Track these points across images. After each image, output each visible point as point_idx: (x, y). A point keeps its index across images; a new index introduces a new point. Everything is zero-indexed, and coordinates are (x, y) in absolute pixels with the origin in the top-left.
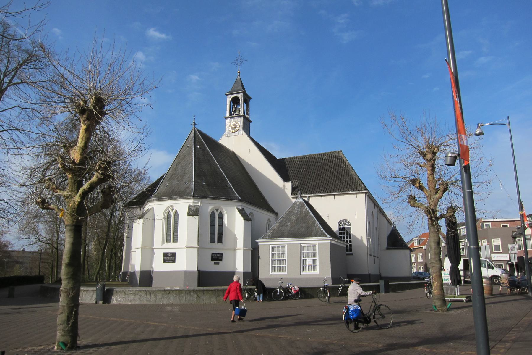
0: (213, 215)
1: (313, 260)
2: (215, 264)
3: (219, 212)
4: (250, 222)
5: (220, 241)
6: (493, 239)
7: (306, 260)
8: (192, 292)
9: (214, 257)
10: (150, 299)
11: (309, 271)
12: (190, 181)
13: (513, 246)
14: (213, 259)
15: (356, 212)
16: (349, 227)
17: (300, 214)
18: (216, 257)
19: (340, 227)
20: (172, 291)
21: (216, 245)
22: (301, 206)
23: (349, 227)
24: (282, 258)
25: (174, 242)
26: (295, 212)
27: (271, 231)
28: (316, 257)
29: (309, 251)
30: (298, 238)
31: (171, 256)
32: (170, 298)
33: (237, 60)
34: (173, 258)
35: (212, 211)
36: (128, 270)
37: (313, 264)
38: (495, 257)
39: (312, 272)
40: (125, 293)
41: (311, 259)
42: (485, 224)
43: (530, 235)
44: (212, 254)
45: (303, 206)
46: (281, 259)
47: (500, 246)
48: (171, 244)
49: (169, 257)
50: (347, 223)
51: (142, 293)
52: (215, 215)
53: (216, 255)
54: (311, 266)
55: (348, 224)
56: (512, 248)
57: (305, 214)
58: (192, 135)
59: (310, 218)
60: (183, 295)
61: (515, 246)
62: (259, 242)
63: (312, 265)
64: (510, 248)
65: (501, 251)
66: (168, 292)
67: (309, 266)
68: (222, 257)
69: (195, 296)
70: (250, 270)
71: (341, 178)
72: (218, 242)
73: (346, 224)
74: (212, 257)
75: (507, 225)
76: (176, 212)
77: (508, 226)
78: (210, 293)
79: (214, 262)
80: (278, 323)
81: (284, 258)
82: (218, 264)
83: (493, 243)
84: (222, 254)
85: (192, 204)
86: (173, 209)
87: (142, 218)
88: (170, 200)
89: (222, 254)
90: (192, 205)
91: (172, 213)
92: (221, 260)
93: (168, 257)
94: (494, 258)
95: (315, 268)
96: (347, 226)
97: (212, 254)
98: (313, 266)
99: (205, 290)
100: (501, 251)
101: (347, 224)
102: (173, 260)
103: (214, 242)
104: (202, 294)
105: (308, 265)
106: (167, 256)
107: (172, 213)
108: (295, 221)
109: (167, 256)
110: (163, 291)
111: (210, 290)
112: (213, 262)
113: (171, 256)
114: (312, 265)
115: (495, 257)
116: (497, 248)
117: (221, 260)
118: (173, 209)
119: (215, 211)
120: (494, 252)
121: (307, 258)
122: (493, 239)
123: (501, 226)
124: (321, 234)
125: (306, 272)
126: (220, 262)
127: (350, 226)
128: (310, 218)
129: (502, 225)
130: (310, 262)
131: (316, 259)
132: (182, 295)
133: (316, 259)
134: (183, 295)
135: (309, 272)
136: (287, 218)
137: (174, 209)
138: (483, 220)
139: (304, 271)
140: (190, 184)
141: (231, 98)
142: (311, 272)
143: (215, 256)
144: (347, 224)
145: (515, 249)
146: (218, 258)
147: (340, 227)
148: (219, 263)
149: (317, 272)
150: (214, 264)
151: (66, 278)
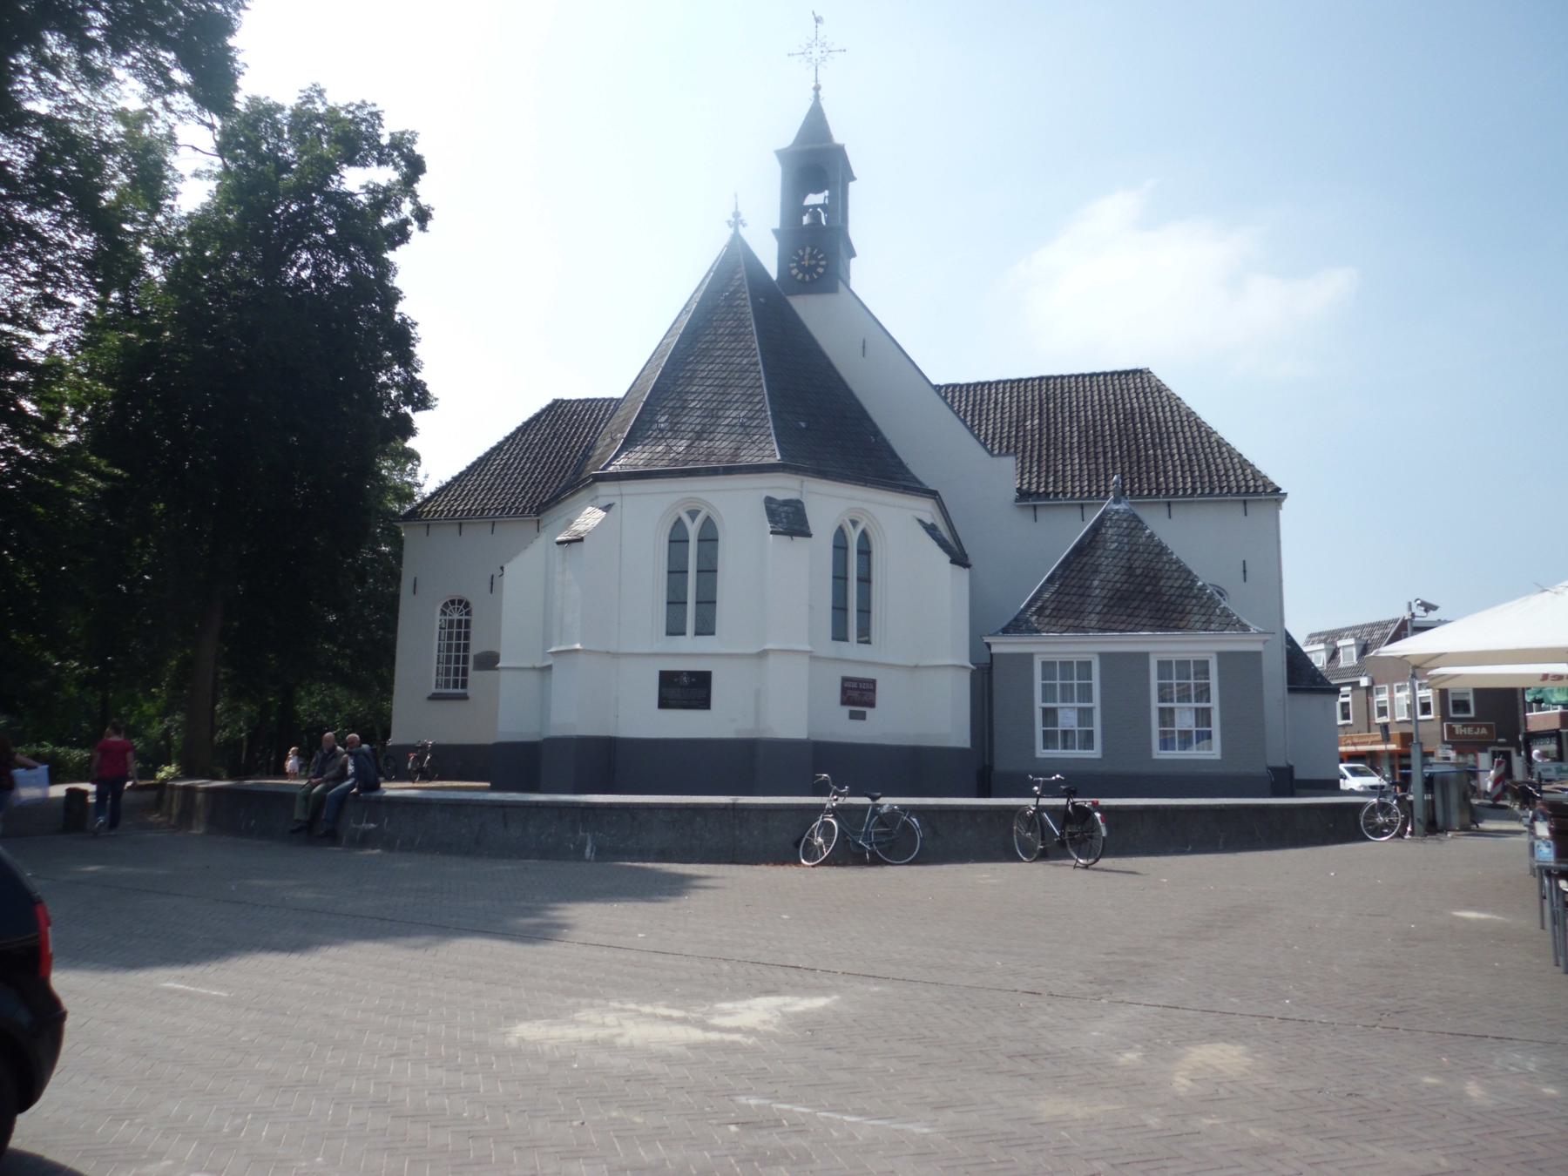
0: (677, 539)
1: (1080, 710)
2: (853, 715)
3: (700, 519)
4: (967, 569)
5: (865, 635)
7: (1172, 710)
9: (850, 693)
14: (846, 700)
16: (467, 617)
21: (852, 649)
23: (467, 617)
35: (834, 530)
41: (1074, 708)
44: (845, 680)
47: (1386, 707)
50: (461, 607)
52: (688, 536)
53: (855, 685)
54: (1074, 731)
62: (995, 643)
65: (1472, 714)
67: (1065, 733)
68: (874, 691)
74: (844, 690)
80: (1442, 766)
82: (862, 716)
84: (873, 682)
86: (854, 523)
89: (873, 682)
91: (693, 530)
92: (872, 704)
95: (1087, 741)
96: (462, 615)
97: (845, 680)
101: (462, 611)
103: (845, 639)
107: (693, 530)
112: (847, 709)
117: (872, 704)
118: (693, 514)
119: (686, 519)
120: (1452, 715)
121: (1058, 704)
126: (868, 710)
137: (698, 512)
143: (851, 689)
144: (458, 609)
148: (864, 713)
149: (1096, 752)
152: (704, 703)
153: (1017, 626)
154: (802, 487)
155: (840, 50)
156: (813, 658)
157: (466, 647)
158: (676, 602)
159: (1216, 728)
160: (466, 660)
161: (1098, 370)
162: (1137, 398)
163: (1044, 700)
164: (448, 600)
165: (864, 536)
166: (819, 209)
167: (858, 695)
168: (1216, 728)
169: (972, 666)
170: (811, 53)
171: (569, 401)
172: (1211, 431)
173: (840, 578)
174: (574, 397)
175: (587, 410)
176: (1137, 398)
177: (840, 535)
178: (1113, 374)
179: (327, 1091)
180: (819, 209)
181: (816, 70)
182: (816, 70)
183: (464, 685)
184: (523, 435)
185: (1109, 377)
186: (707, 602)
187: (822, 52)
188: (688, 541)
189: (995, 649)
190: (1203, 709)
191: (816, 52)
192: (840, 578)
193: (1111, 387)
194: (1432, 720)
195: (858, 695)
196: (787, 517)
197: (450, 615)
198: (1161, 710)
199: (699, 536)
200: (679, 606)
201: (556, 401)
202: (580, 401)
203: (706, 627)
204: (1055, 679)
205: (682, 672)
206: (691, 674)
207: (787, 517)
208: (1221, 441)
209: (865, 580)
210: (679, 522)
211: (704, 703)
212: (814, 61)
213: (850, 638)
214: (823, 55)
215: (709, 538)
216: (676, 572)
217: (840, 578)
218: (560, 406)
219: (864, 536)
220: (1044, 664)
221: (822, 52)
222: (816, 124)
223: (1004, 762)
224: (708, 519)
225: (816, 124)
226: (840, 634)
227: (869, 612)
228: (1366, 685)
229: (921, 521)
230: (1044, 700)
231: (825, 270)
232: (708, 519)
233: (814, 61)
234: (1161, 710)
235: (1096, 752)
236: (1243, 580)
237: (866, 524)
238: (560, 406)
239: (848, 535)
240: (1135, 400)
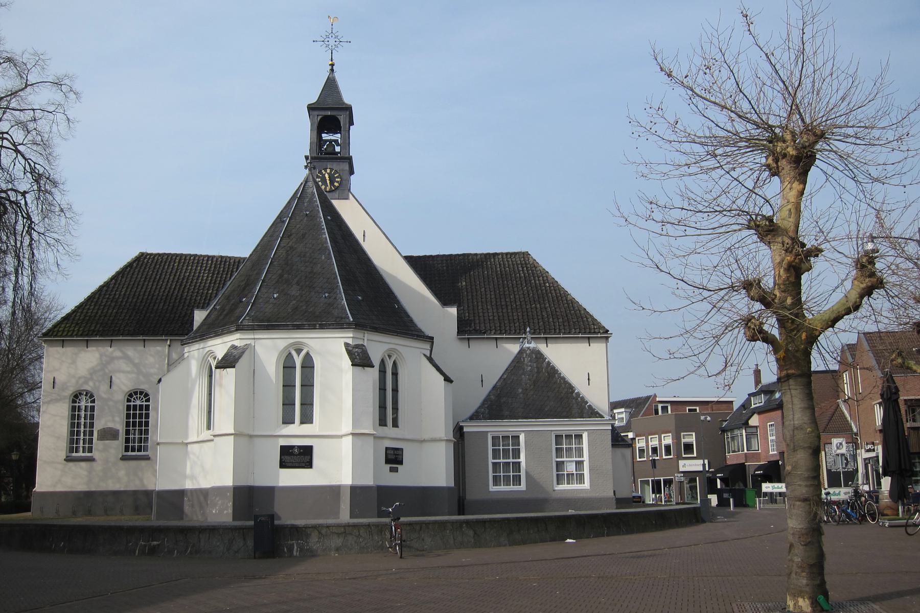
0: (288, 367)
2: (392, 470)
3: (303, 353)
5: (395, 424)
6: (682, 434)
7: (563, 462)
8: (464, 525)
10: (381, 543)
11: (568, 483)
12: (333, 289)
13: (840, 442)
14: (388, 461)
15: (54, 378)
17: (538, 372)
18: (393, 457)
19: (129, 403)
20: (426, 524)
21: (389, 431)
22: (536, 358)
24: (576, 457)
25: (302, 423)
26: (527, 368)
27: (486, 406)
28: (583, 457)
29: (571, 447)
30: (547, 420)
31: (300, 454)
32: (423, 540)
33: (336, 37)
34: (307, 458)
36: (278, 482)
37: (576, 471)
38: (685, 464)
39: (512, 488)
40: (320, 533)
41: (572, 461)
42: (660, 406)
43: (756, 427)
45: (540, 358)
46: (511, 460)
48: (297, 429)
49: (297, 455)
50: (142, 396)
51: (362, 531)
55: (144, 399)
56: (838, 445)
57: (548, 373)
58: (309, 191)
59: (560, 381)
60: (448, 531)
61: (843, 441)
63: (575, 472)
64: (844, 447)
65: (695, 455)
66: (418, 528)
67: (568, 475)
69: (471, 533)
70: (452, 484)
71: (205, 300)
72: (393, 426)
73: (137, 397)
75: (696, 409)
76: (308, 355)
77: (698, 411)
78: (495, 526)
79: (390, 467)
81: (562, 458)
82: (395, 470)
83: (683, 441)
85: (350, 341)
86: (390, 356)
87: (234, 367)
88: (297, 329)
90: (351, 343)
91: (298, 361)
92: (401, 463)
93: (294, 455)
94: (683, 466)
95: (581, 479)
96: (143, 402)
98: (576, 474)
99: (488, 521)
100: (695, 455)
101: (142, 399)
102: (308, 462)
103: (386, 425)
104: (483, 530)
105: (565, 473)
106: (292, 454)
107: (298, 361)
108: (530, 386)
109: (292, 454)
110: (407, 524)
111: (495, 521)
112: (388, 466)
113: (300, 454)
114: (575, 472)
115: (685, 464)
116: (688, 448)
117: (401, 463)
118: (299, 351)
120: (684, 456)
122: (682, 434)
123: (686, 411)
124: (591, 413)
125: (564, 487)
126: (399, 467)
127: (149, 402)
128: (560, 381)
129: (687, 408)
130: (571, 468)
131: (582, 462)
132: (446, 533)
133: (582, 462)
134: (448, 531)
135: (568, 486)
136: (513, 379)
138: (658, 399)
139: (558, 484)
140: (335, 298)
141: (319, 118)
142: (573, 485)
144: (140, 397)
145: (842, 447)
146: (396, 458)
147: (129, 403)
149: (586, 485)
150: (390, 471)
151: (812, 475)
152: (309, 465)
153: (475, 417)
154: (364, 337)
155: (347, 42)
156: (353, 434)
157: (92, 425)
158: (288, 403)
159: (586, 472)
160: (91, 433)
161: (498, 251)
162: (523, 270)
163: (494, 458)
164: (127, 397)
165: (395, 364)
166: (333, 143)
167: (394, 458)
168: (586, 472)
169: (454, 439)
170: (328, 41)
171: (151, 254)
172: (567, 294)
173: (382, 389)
174: (155, 251)
175: (166, 262)
176: (523, 270)
177: (383, 362)
178: (507, 254)
179: (802, 436)
180: (333, 143)
181: (332, 53)
182: (332, 53)
183: (90, 450)
184: (122, 277)
185: (505, 256)
186: (308, 404)
187: (336, 41)
188: (295, 367)
189: (465, 430)
190: (516, 462)
191: (332, 42)
192: (382, 389)
193: (507, 263)
194: (645, 461)
195: (394, 458)
196: (358, 355)
197: (79, 403)
198: (494, 464)
199: (302, 364)
200: (290, 406)
201: (142, 254)
202: (159, 255)
203: (307, 418)
204: (131, 411)
205: (295, 446)
206: (300, 447)
207: (358, 355)
208: (573, 300)
209: (395, 390)
210: (290, 356)
211: (309, 465)
212: (330, 47)
213: (388, 425)
214: (337, 43)
215: (308, 365)
216: (288, 386)
217: (382, 389)
218: (145, 258)
219: (395, 364)
220: (493, 438)
221: (336, 41)
222: (331, 86)
223: (472, 494)
224: (308, 354)
225: (331, 86)
226: (383, 422)
227: (397, 409)
228: (632, 437)
229: (425, 355)
230: (494, 458)
231: (340, 184)
232: (308, 354)
233: (330, 47)
234: (494, 464)
235: (523, 487)
236: (366, 231)
237: (396, 357)
238: (145, 258)
239: (386, 362)
240: (521, 272)
